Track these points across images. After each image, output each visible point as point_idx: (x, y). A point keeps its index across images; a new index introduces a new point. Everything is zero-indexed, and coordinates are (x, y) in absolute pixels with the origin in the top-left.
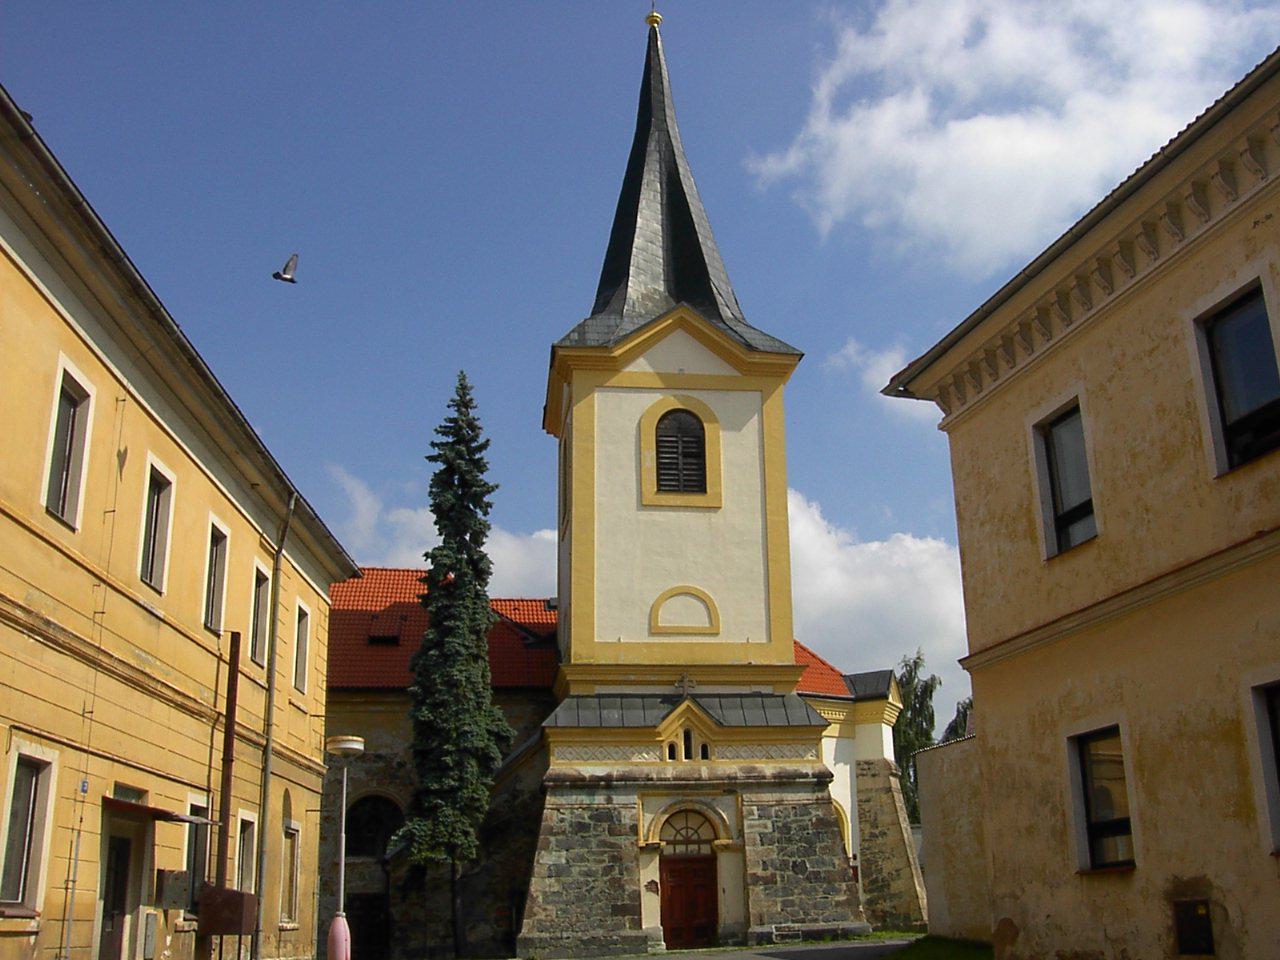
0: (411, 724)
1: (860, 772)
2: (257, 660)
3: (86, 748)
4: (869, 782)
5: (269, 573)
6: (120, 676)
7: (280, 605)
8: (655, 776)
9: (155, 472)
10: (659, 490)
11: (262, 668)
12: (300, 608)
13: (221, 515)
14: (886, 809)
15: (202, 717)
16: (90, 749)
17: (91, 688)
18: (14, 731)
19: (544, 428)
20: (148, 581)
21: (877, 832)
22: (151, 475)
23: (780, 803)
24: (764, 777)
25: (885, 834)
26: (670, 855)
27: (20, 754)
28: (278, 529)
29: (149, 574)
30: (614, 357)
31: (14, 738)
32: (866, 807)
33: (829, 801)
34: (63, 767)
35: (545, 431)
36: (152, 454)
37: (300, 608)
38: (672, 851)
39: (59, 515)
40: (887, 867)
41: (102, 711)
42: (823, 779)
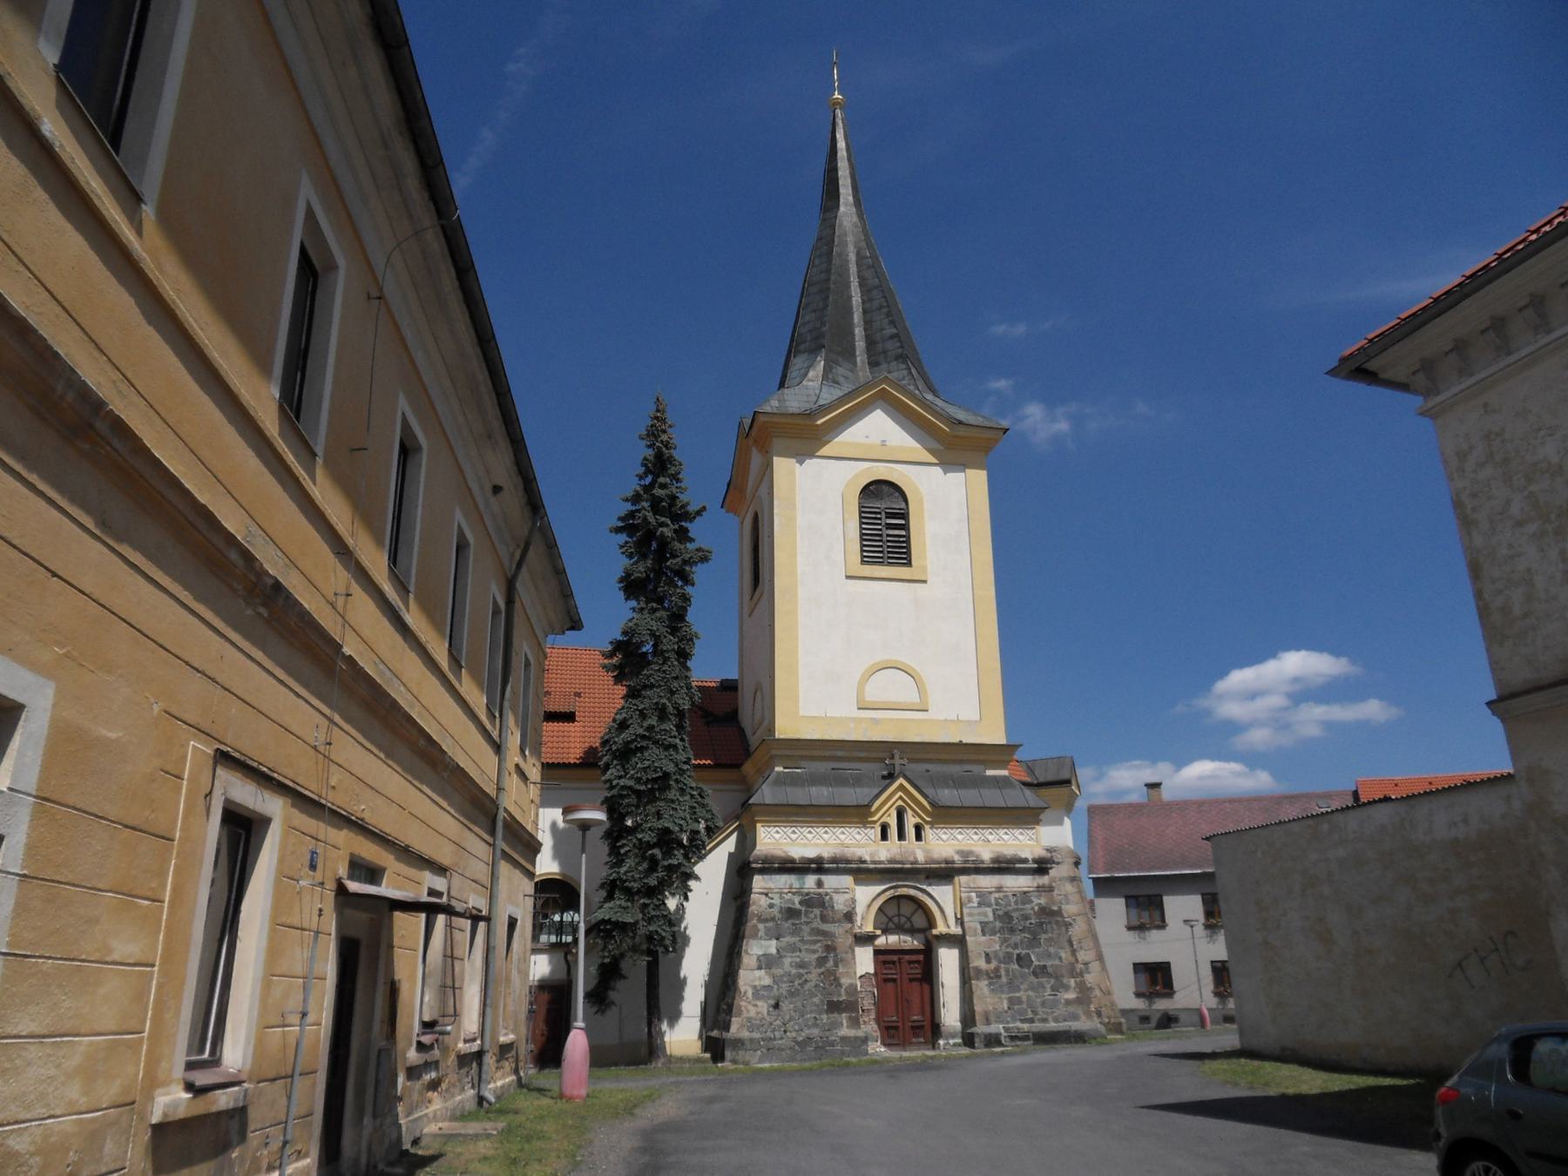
8: (868, 858)
10: (863, 562)
23: (999, 889)
24: (982, 862)
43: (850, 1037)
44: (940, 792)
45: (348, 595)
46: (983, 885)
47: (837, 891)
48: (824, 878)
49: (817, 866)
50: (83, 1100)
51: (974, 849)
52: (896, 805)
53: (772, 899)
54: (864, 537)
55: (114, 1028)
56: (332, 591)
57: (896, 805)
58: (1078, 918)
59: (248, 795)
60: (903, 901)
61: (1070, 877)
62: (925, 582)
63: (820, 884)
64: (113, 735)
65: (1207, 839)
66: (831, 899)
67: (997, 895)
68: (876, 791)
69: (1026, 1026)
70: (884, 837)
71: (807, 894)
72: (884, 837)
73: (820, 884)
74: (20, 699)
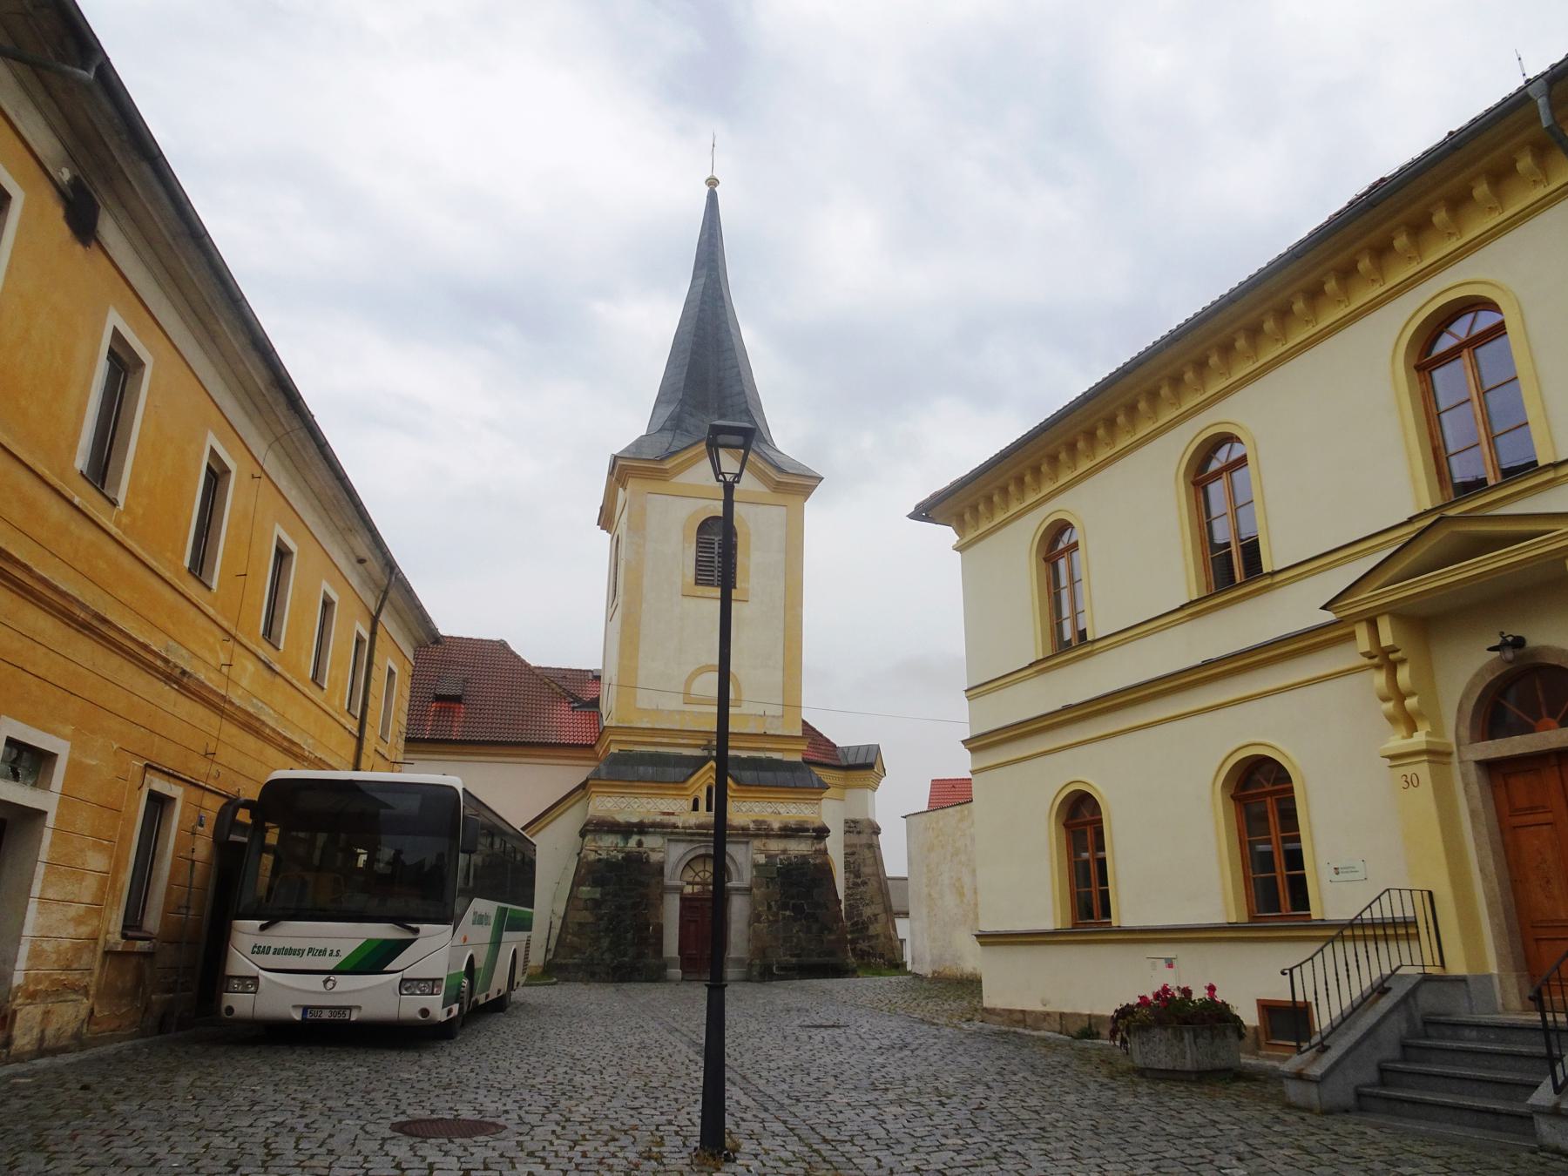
0: (684, 986)
1: (847, 829)
2: (318, 681)
3: (203, 784)
4: (854, 839)
5: (366, 636)
6: (240, 722)
7: (374, 666)
8: (680, 825)
9: (390, 669)
10: (697, 584)
11: (356, 718)
12: (389, 668)
13: (330, 581)
14: (868, 862)
15: (304, 761)
16: (207, 786)
17: (215, 733)
18: (148, 769)
19: (598, 525)
20: (197, 574)
21: (859, 881)
22: (277, 547)
23: (784, 852)
24: (772, 830)
25: (866, 883)
26: (689, 894)
27: (150, 790)
28: (378, 598)
29: (269, 633)
30: (666, 469)
31: (147, 775)
32: (851, 859)
33: (825, 852)
34: (186, 803)
35: (599, 527)
36: (326, 584)
37: (389, 668)
38: (691, 891)
39: (99, 486)
40: (868, 912)
41: (224, 755)
42: (822, 833)
43: (57, 812)
44: (743, 773)
45: (230, 665)
46: (772, 849)
47: (653, 850)
48: (643, 839)
49: (642, 828)
50: (74, 933)
51: (766, 819)
52: (708, 781)
53: (600, 855)
54: (700, 563)
55: (88, 902)
56: (262, 479)
57: (708, 781)
58: (872, 878)
59: (161, 785)
60: (691, 864)
61: (867, 844)
62: (747, 601)
63: (640, 844)
64: (94, 763)
65: (905, 817)
66: (648, 856)
67: (782, 857)
68: (691, 771)
69: (794, 960)
70: (695, 807)
71: (629, 852)
72: (695, 807)
73: (640, 844)
74: (55, 752)
